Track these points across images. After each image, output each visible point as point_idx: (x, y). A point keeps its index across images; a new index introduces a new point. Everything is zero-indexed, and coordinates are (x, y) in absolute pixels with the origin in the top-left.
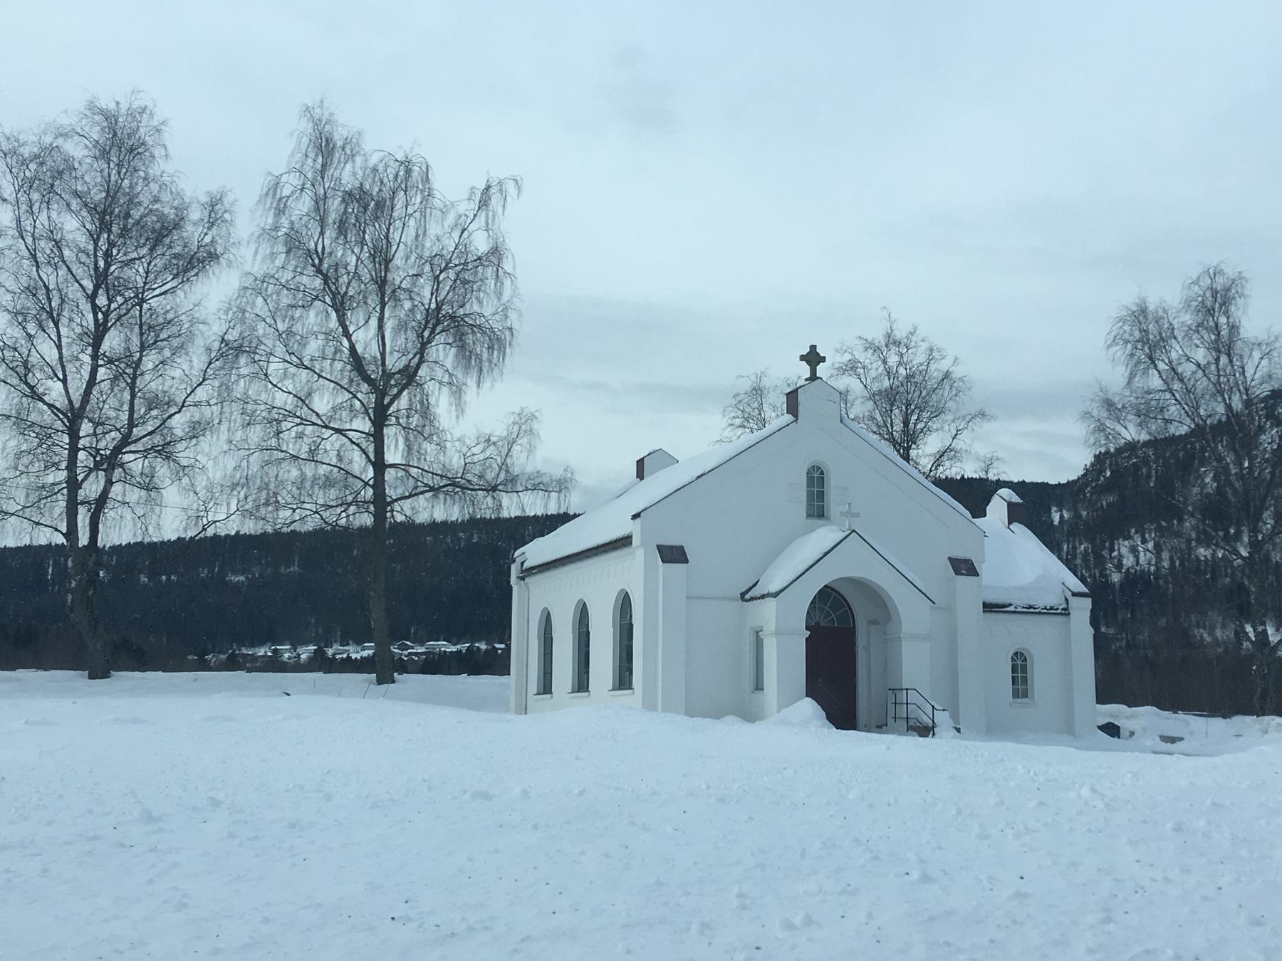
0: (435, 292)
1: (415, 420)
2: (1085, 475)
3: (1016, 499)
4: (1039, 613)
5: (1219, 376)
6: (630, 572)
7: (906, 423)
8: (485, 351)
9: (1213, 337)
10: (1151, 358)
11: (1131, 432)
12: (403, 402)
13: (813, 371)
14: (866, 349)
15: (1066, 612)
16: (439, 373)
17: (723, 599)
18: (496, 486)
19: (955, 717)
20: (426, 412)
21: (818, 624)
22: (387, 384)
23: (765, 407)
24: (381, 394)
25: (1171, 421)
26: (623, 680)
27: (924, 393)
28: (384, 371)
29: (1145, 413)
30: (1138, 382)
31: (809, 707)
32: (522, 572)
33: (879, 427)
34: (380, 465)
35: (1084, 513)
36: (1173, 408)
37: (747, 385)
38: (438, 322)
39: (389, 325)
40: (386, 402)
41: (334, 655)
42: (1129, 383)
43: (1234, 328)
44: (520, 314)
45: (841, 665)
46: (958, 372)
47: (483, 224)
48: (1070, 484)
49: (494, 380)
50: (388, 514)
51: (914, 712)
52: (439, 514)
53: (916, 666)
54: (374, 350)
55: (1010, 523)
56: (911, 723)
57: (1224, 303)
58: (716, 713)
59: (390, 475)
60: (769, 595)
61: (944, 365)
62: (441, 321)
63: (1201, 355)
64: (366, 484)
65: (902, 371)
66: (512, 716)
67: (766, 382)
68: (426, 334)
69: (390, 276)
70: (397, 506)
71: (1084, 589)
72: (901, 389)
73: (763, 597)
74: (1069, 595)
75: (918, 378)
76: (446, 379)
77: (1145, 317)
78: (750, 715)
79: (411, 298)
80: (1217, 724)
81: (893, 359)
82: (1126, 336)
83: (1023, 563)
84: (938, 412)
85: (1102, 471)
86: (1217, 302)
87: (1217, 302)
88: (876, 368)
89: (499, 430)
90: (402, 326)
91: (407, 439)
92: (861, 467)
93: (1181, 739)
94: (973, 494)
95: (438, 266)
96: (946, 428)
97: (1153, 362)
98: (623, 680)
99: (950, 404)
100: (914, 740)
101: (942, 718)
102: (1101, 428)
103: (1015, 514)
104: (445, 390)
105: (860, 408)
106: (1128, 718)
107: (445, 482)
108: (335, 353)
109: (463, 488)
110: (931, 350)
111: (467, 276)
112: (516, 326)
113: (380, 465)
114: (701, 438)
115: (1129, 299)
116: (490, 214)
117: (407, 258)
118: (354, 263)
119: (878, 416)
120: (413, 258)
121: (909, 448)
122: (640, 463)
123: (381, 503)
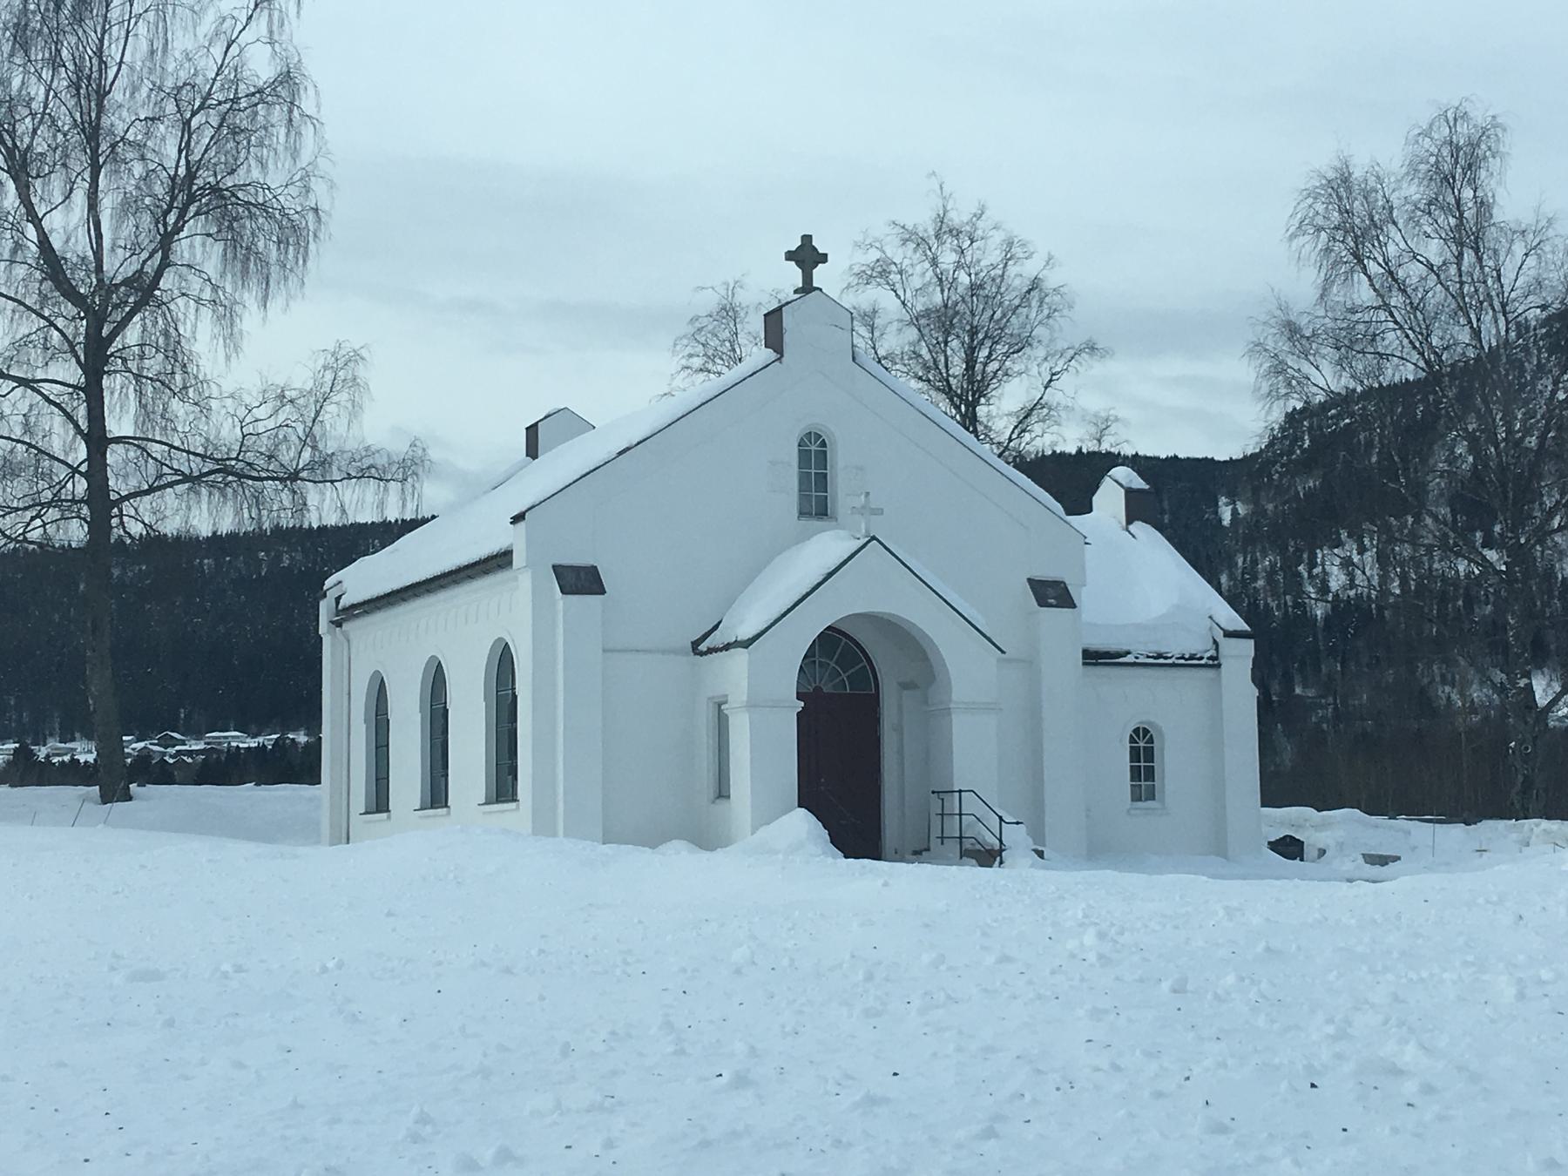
0: (185, 148)
1: (154, 364)
2: (1271, 444)
3: (1139, 483)
4: (1174, 665)
5: (1462, 283)
6: (513, 610)
7: (970, 362)
8: (274, 248)
9: (1453, 221)
10: (1356, 255)
11: (1327, 377)
12: (132, 335)
13: (808, 278)
14: (905, 241)
15: (1215, 663)
16: (195, 284)
17: (664, 652)
18: (297, 472)
19: (1038, 834)
20: (173, 349)
21: (818, 689)
22: (106, 300)
23: (742, 339)
24: (96, 319)
25: (1387, 357)
26: (503, 786)
27: (998, 315)
28: (100, 281)
29: (1351, 341)
30: (1337, 294)
31: (802, 823)
32: (338, 613)
33: (927, 369)
34: (97, 439)
35: (1270, 507)
36: (1391, 336)
37: (709, 301)
38: (192, 199)
39: (107, 204)
40: (105, 332)
41: (48, 756)
42: (1322, 296)
43: (1483, 206)
44: (332, 186)
45: (856, 756)
46: (1052, 280)
47: (264, 31)
48: (1248, 460)
49: (289, 297)
50: (114, 522)
51: (973, 829)
52: (203, 525)
53: (975, 755)
54: (81, 245)
55: (1129, 521)
56: (967, 844)
57: (1470, 166)
58: (652, 839)
59: (114, 455)
60: (738, 644)
61: (1030, 268)
62: (198, 196)
63: (1434, 250)
64: (75, 470)
65: (964, 279)
66: (326, 851)
67: (742, 298)
68: (171, 218)
69: (105, 121)
70: (127, 508)
71: (1243, 626)
72: (961, 307)
73: (727, 647)
74: (1219, 635)
75: (990, 289)
76: (207, 294)
77: (1349, 190)
78: (707, 839)
79: (143, 158)
80: (1457, 831)
81: (948, 259)
82: (1319, 221)
83: (1146, 584)
84: (1021, 345)
85: (1297, 439)
86: (1457, 164)
87: (1457, 164)
88: (920, 274)
89: (300, 379)
90: (128, 207)
91: (140, 393)
92: (893, 438)
93: (1399, 858)
94: (1071, 479)
95: (187, 102)
96: (1035, 370)
97: (1360, 261)
98: (503, 786)
99: (1039, 331)
100: (971, 874)
101: (1016, 837)
102: (1279, 369)
103: (1138, 506)
104: (206, 313)
105: (896, 340)
106: (1315, 827)
107: (210, 466)
108: (14, 251)
109: (241, 476)
110: (1010, 244)
111: (241, 120)
112: (324, 205)
113: (97, 439)
114: (631, 388)
115: (1323, 161)
116: (276, 14)
117: (135, 89)
118: (41, 97)
119: (924, 352)
120: (144, 91)
121: (976, 403)
122: (532, 431)
123: (101, 503)
